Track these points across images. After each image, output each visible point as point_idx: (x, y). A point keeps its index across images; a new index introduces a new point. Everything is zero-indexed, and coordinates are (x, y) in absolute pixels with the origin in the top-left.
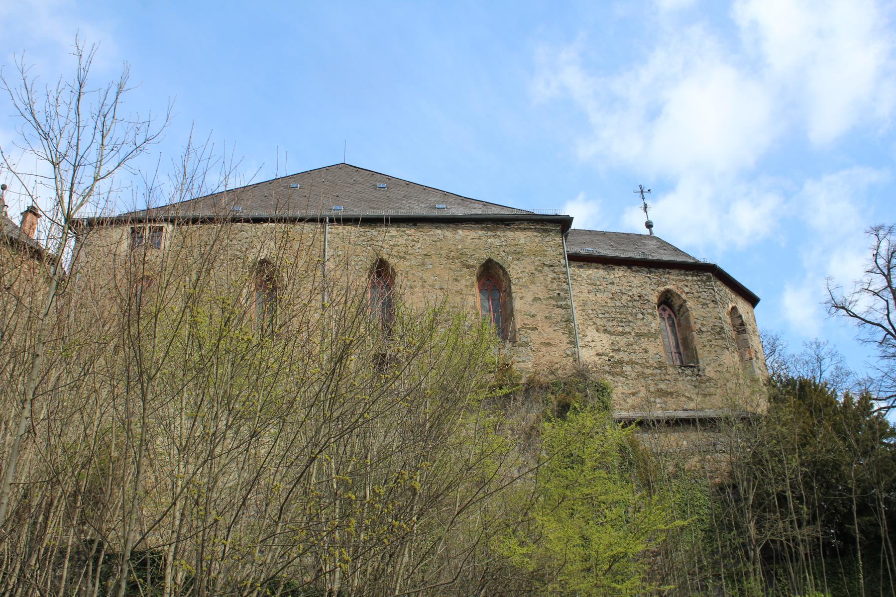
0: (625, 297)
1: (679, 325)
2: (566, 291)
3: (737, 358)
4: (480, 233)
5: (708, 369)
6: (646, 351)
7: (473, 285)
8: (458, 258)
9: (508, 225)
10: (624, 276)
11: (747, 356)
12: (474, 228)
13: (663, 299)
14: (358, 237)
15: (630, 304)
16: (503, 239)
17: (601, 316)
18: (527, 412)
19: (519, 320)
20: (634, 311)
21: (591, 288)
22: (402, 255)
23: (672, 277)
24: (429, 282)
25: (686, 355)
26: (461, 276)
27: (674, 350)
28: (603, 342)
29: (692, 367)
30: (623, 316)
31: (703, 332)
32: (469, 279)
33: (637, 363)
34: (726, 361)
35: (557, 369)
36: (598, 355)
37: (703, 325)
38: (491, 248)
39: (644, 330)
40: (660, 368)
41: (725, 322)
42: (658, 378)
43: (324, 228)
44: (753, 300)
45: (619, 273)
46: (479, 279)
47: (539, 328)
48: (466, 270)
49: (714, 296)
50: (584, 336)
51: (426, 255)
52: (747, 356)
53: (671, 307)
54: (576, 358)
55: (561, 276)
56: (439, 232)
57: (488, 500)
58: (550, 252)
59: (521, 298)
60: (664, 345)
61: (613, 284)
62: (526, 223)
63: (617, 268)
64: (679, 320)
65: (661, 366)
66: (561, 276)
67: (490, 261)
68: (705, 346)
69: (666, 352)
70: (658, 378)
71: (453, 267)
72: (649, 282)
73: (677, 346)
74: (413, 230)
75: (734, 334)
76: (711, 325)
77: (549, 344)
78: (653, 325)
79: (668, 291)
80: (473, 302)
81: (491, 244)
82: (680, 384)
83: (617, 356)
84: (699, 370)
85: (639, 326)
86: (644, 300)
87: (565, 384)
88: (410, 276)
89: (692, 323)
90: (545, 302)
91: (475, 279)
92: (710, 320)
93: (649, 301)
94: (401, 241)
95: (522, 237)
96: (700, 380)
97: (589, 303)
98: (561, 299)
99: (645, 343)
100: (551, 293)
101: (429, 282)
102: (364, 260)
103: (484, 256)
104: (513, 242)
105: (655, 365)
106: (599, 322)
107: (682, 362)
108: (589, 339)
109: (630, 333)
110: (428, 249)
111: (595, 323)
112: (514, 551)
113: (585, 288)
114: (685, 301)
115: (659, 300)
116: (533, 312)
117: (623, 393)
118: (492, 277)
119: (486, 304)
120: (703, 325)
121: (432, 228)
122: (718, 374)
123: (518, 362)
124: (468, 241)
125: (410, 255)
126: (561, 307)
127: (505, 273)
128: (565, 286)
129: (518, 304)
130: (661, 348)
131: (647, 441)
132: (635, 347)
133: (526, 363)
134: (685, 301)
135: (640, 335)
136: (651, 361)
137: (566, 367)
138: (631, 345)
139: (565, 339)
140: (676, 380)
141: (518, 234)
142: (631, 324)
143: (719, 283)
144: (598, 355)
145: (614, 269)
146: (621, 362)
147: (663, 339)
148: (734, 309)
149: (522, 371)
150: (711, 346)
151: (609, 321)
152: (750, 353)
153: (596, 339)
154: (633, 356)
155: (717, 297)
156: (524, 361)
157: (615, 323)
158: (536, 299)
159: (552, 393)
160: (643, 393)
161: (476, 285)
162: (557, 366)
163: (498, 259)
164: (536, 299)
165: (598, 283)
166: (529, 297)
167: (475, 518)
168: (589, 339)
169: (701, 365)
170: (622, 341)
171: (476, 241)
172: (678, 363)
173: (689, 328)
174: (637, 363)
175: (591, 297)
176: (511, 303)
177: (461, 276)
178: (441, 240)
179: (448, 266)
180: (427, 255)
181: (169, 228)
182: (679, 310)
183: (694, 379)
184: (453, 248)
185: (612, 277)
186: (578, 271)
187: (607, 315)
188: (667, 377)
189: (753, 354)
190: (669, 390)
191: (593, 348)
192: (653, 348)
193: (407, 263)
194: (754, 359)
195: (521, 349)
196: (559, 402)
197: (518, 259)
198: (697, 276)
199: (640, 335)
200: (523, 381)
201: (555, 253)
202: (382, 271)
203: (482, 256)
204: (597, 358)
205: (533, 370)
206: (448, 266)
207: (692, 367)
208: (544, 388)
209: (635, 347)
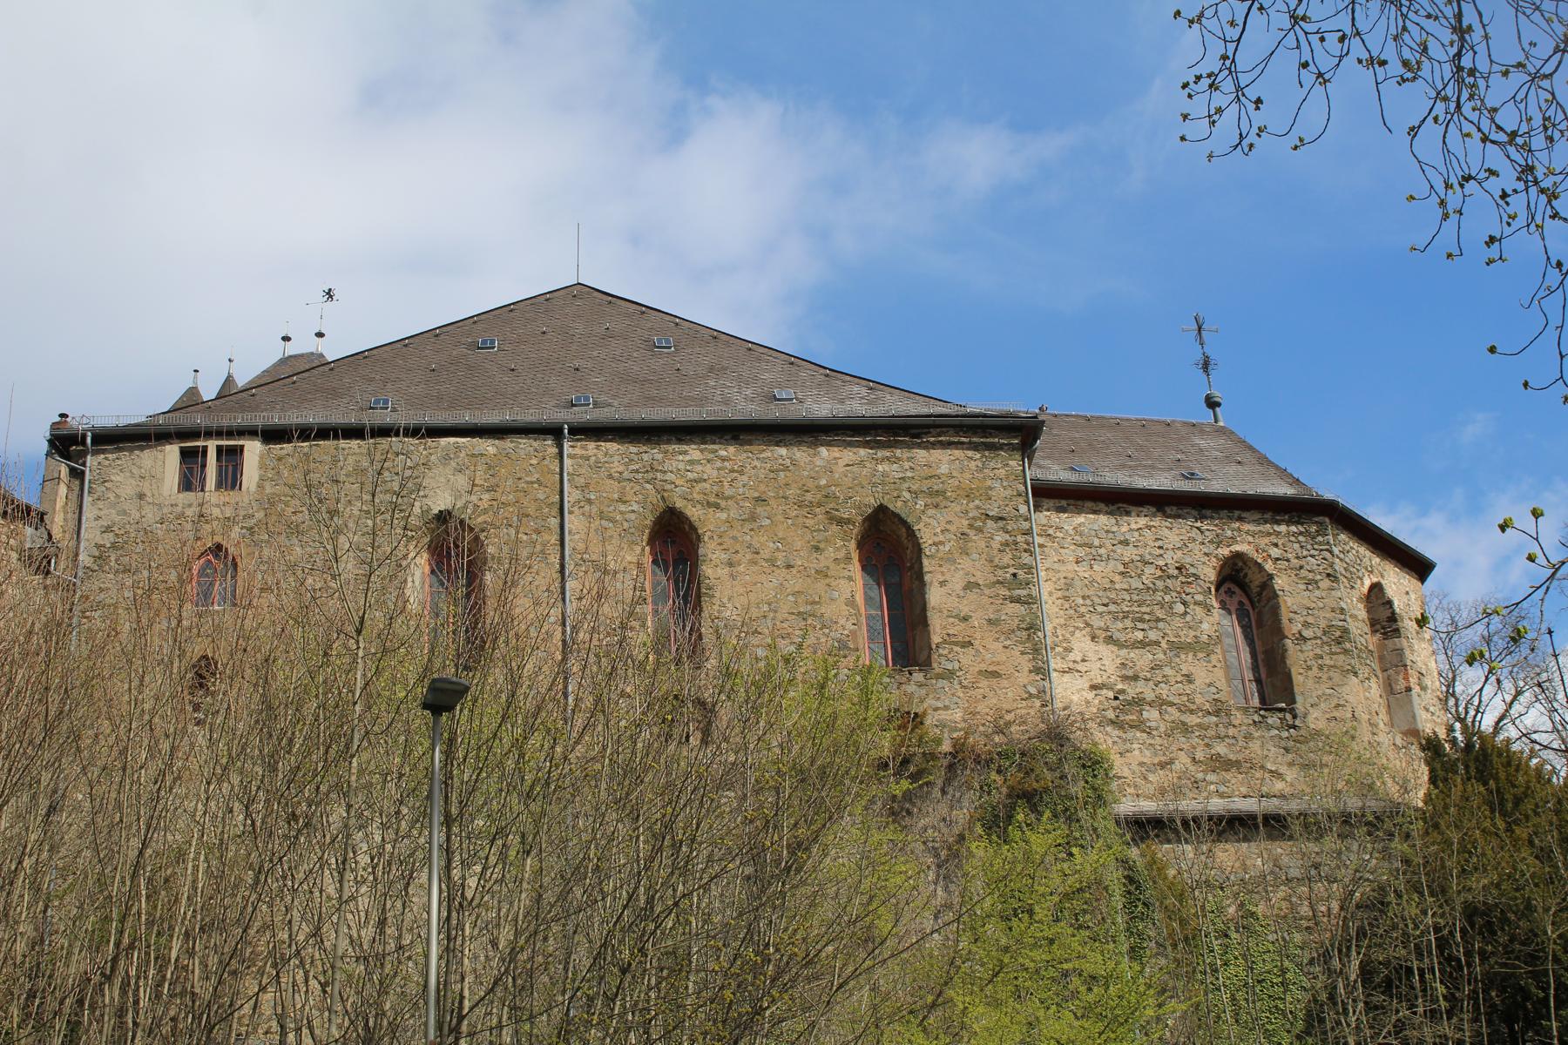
0: (1149, 570)
1: (1260, 624)
2: (1029, 569)
3: (1375, 689)
4: (863, 452)
6: (1189, 678)
7: (848, 559)
8: (820, 505)
9: (917, 436)
10: (1149, 527)
11: (1402, 685)
12: (850, 444)
13: (1227, 571)
15: (1160, 584)
16: (907, 465)
17: (1100, 609)
18: (952, 807)
19: (938, 628)
20: (1167, 598)
21: (1081, 552)
23: (1246, 527)
24: (765, 554)
25: (1273, 684)
26: (827, 540)
27: (1249, 675)
28: (1104, 661)
29: (1281, 710)
30: (1144, 609)
31: (1305, 639)
32: (843, 549)
33: (1172, 704)
34: (1351, 698)
35: (1008, 724)
36: (1093, 687)
37: (1306, 625)
38: (883, 484)
39: (1188, 636)
40: (1217, 713)
42: (1211, 733)
43: (560, 447)
44: (1419, 567)
45: (1136, 523)
47: (976, 643)
50: (1066, 649)
51: (758, 499)
52: (1402, 685)
53: (1243, 586)
55: (1020, 538)
56: (783, 451)
58: (1000, 491)
60: (1227, 667)
61: (1125, 543)
62: (951, 432)
63: (1134, 510)
64: (1260, 614)
65: (1219, 709)
66: (1020, 538)
67: (882, 509)
68: (1309, 668)
69: (1229, 680)
70: (1211, 733)
71: (810, 522)
72: (1200, 538)
74: (732, 449)
75: (1373, 641)
76: (1323, 624)
77: (995, 674)
78: (1205, 626)
79: (1238, 556)
80: (849, 595)
82: (1255, 746)
83: (1132, 691)
84: (1295, 717)
85: (1175, 629)
87: (1023, 754)
88: (728, 542)
89: (1285, 621)
90: (987, 592)
91: (853, 545)
93: (1197, 577)
94: (710, 471)
95: (945, 462)
97: (1077, 583)
98: (1017, 586)
99: (1187, 663)
100: (1000, 572)
101: (765, 554)
102: (638, 512)
103: (870, 500)
106: (1097, 622)
107: (1263, 700)
108: (1076, 655)
109: (1157, 643)
110: (762, 487)
111: (1088, 624)
113: (1069, 554)
114: (1271, 577)
116: (965, 611)
117: (1141, 764)
118: (888, 548)
119: (875, 593)
120: (1306, 625)
122: (1333, 723)
123: (936, 709)
124: (840, 469)
125: (727, 499)
126: (1017, 600)
127: (911, 534)
128: (1026, 559)
129: (935, 596)
131: (1181, 858)
132: (1168, 671)
133: (950, 710)
134: (1271, 577)
135: (1178, 647)
136: (1199, 700)
137: (1026, 722)
138: (1160, 667)
139: (1025, 663)
140: (1248, 737)
141: (937, 454)
142: (1161, 625)
143: (1343, 537)
144: (1093, 687)
145: (1128, 513)
146: (1138, 702)
147: (1224, 652)
148: (1376, 588)
149: (942, 725)
150: (1321, 668)
151: (1116, 619)
152: (1406, 679)
153: (1091, 656)
154: (1164, 690)
155: (1339, 566)
156: (946, 708)
157: (1128, 623)
158: (970, 586)
159: (999, 772)
160: (1183, 761)
161: (855, 556)
162: (1009, 717)
163: (896, 506)
164: (970, 586)
165: (1096, 542)
166: (957, 583)
168: (1076, 655)
169: (1299, 707)
170: (1142, 659)
171: (855, 469)
172: (1256, 702)
173: (1278, 632)
174: (1172, 704)
175: (1083, 570)
176: (923, 594)
177: (827, 540)
179: (800, 520)
180: (760, 500)
181: (253, 450)
182: (1260, 594)
183: (1285, 734)
184: (811, 484)
185: (1124, 529)
187: (1112, 608)
188: (1231, 731)
189: (1413, 681)
190: (1231, 757)
193: (724, 516)
194: (1416, 689)
195: (941, 683)
197: (937, 506)
199: (1178, 647)
200: (946, 747)
201: (1009, 492)
202: (674, 539)
204: (1090, 695)
205: (963, 725)
206: (800, 520)
207: (1281, 710)
209: (1168, 671)
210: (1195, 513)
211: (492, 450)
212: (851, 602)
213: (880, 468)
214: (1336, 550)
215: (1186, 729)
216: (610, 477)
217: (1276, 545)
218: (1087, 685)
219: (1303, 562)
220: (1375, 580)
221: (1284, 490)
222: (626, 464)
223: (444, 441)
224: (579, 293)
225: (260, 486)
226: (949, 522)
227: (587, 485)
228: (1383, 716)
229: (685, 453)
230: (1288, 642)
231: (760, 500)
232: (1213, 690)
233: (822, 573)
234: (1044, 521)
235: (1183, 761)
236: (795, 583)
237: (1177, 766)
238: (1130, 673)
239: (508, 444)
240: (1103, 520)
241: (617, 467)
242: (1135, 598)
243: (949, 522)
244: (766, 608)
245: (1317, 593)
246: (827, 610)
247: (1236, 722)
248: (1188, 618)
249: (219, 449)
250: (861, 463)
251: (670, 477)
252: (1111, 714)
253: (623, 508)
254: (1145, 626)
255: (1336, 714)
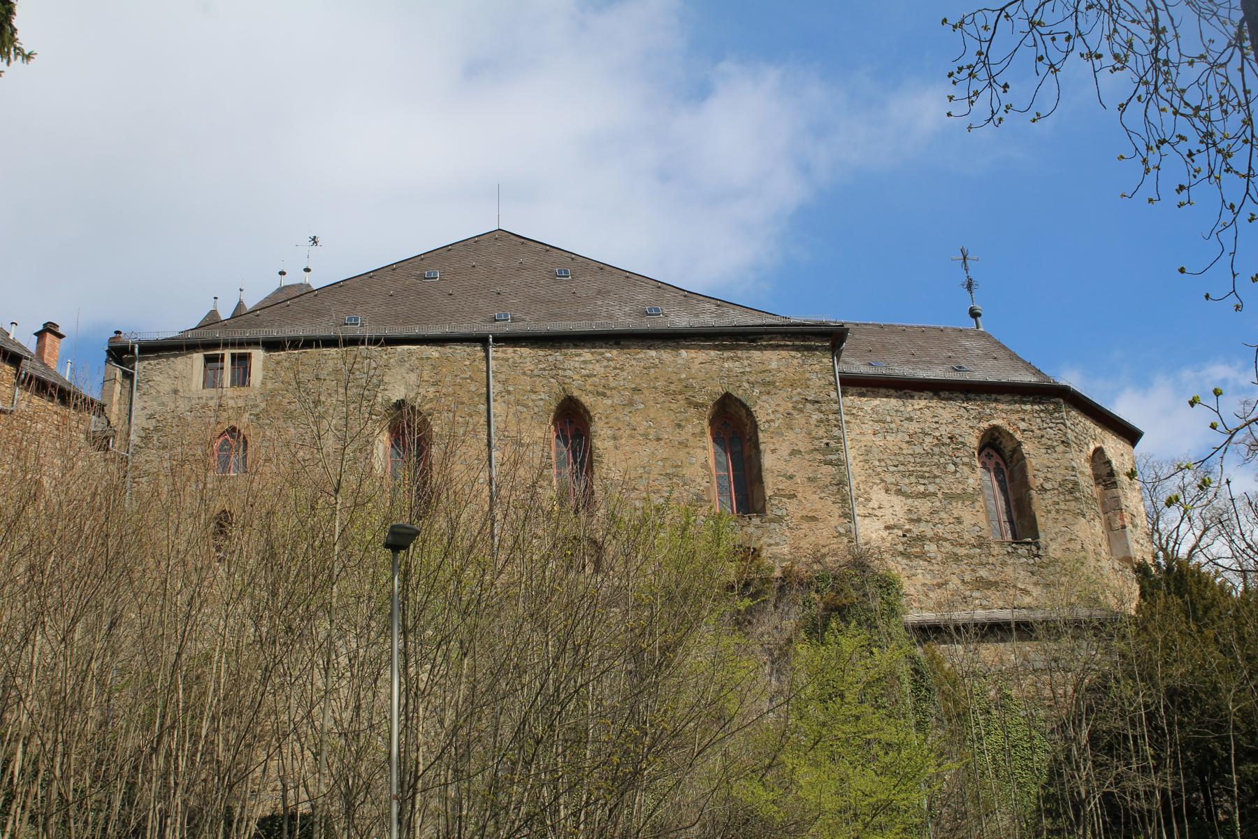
0: (928, 440)
1: (1012, 479)
2: (838, 440)
3: (1098, 527)
4: (713, 353)
5: (1053, 546)
6: (959, 520)
7: (703, 433)
8: (681, 393)
9: (754, 341)
11: (1118, 524)
12: (703, 348)
13: (987, 440)
14: (536, 364)
15: (936, 450)
16: (746, 362)
17: (892, 469)
18: (782, 619)
20: (942, 460)
21: (877, 427)
22: (600, 390)
23: (1001, 406)
24: (641, 430)
25: (1022, 524)
26: (686, 420)
27: (1004, 517)
28: (895, 509)
30: (925, 469)
31: (1046, 490)
32: (698, 429)
33: (947, 540)
34: (1080, 534)
35: (824, 556)
36: (887, 528)
37: (1046, 479)
38: (728, 376)
40: (980, 546)
41: (1082, 473)
42: (976, 561)
44: (1131, 435)
45: (918, 404)
46: (711, 423)
47: (799, 495)
48: (692, 410)
49: (1065, 434)
51: (634, 389)
52: (1118, 524)
53: (999, 451)
54: (851, 536)
55: (831, 417)
56: (653, 353)
57: (729, 741)
58: (816, 382)
59: (773, 451)
60: (987, 512)
61: (910, 419)
62: (779, 337)
63: (917, 394)
65: (981, 543)
66: (831, 417)
67: (727, 396)
68: (1049, 512)
69: (989, 521)
70: (976, 561)
71: (673, 406)
72: (966, 415)
73: (1008, 512)
74: (615, 352)
75: (1096, 491)
76: (1059, 479)
77: (814, 519)
78: (971, 481)
79: (995, 428)
80: (704, 460)
81: (729, 370)
82: (1009, 570)
83: (916, 530)
84: (1038, 548)
85: (948, 483)
86: (957, 444)
87: (835, 578)
89: (1030, 477)
90: (807, 457)
91: (706, 423)
92: (1058, 471)
93: (964, 444)
94: (599, 369)
95: (774, 360)
96: (1040, 564)
97: (875, 450)
99: (958, 509)
100: (816, 442)
101: (641, 430)
102: (545, 399)
103: (719, 390)
104: (761, 367)
105: (973, 541)
106: (890, 479)
109: (935, 494)
110: (638, 380)
111: (883, 481)
112: (755, 795)
113: (868, 428)
114: (1020, 444)
115: (981, 442)
116: (791, 471)
117: (924, 585)
118: (733, 425)
119: (723, 459)
120: (1046, 479)
121: (642, 348)
123: (770, 545)
124: (696, 366)
125: (611, 389)
126: (830, 463)
127: (750, 414)
128: (836, 432)
129: (768, 461)
130: (982, 516)
131: (955, 654)
132: (943, 515)
133: (780, 545)
134: (1020, 444)
135: (950, 497)
137: (836, 554)
140: (1004, 564)
141: (768, 354)
142: (938, 480)
143: (1073, 413)
144: (887, 528)
145: (912, 397)
146: (921, 538)
147: (985, 500)
148: (1099, 452)
149: (774, 557)
150: (1057, 511)
151: (904, 476)
152: (1122, 519)
153: (885, 504)
154: (940, 529)
155: (1071, 435)
156: (777, 544)
157: (913, 479)
158: (794, 453)
159: (817, 592)
160: (955, 582)
161: (708, 431)
162: (824, 551)
163: (738, 394)
164: (794, 453)
165: (889, 419)
166: (784, 451)
167: (716, 761)
169: (1042, 541)
170: (924, 506)
171: (707, 366)
172: (1009, 537)
173: (1025, 485)
174: (947, 540)
175: (878, 440)
177: (686, 420)
178: (656, 366)
179: (667, 404)
180: (636, 390)
182: (1011, 457)
183: (1031, 561)
184: (674, 378)
185: (909, 409)
186: (857, 401)
187: (901, 468)
188: (991, 560)
189: (1127, 521)
191: (877, 522)
192: (970, 517)
193: (609, 402)
194: (1129, 527)
195: (773, 525)
196: (826, 604)
198: (1039, 403)
199: (950, 497)
200: (777, 573)
201: (823, 382)
202: (572, 420)
203: (716, 390)
204: (885, 534)
206: (667, 404)
207: (1028, 543)
208: (806, 584)
209: (943, 515)
210: (962, 396)
211: (436, 355)
212: (705, 466)
213: (726, 365)
214: (1068, 423)
215: (957, 558)
216: (524, 374)
217: (1023, 420)
218: (882, 526)
219: (1043, 433)
220: (1098, 445)
221: (1028, 378)
222: (536, 364)
223: (400, 348)
224: (500, 236)
225: (263, 383)
226: (778, 405)
227: (507, 380)
228: (1105, 547)
229: (580, 355)
230: (1033, 492)
231: (636, 390)
232: (977, 528)
233: (683, 444)
234: (849, 404)
235: (955, 582)
236: (663, 452)
237: (951, 586)
238: (915, 517)
239: (448, 350)
240: (893, 402)
241: (529, 366)
242: (918, 460)
243: (778, 405)
244: (641, 470)
245: (1055, 455)
246: (687, 472)
247: (995, 553)
248: (958, 475)
249: (233, 356)
250: (712, 362)
251: (569, 373)
252: (901, 548)
253: (534, 397)
254: (926, 481)
255: (1069, 546)
